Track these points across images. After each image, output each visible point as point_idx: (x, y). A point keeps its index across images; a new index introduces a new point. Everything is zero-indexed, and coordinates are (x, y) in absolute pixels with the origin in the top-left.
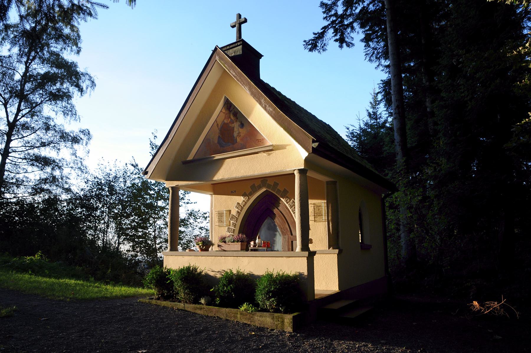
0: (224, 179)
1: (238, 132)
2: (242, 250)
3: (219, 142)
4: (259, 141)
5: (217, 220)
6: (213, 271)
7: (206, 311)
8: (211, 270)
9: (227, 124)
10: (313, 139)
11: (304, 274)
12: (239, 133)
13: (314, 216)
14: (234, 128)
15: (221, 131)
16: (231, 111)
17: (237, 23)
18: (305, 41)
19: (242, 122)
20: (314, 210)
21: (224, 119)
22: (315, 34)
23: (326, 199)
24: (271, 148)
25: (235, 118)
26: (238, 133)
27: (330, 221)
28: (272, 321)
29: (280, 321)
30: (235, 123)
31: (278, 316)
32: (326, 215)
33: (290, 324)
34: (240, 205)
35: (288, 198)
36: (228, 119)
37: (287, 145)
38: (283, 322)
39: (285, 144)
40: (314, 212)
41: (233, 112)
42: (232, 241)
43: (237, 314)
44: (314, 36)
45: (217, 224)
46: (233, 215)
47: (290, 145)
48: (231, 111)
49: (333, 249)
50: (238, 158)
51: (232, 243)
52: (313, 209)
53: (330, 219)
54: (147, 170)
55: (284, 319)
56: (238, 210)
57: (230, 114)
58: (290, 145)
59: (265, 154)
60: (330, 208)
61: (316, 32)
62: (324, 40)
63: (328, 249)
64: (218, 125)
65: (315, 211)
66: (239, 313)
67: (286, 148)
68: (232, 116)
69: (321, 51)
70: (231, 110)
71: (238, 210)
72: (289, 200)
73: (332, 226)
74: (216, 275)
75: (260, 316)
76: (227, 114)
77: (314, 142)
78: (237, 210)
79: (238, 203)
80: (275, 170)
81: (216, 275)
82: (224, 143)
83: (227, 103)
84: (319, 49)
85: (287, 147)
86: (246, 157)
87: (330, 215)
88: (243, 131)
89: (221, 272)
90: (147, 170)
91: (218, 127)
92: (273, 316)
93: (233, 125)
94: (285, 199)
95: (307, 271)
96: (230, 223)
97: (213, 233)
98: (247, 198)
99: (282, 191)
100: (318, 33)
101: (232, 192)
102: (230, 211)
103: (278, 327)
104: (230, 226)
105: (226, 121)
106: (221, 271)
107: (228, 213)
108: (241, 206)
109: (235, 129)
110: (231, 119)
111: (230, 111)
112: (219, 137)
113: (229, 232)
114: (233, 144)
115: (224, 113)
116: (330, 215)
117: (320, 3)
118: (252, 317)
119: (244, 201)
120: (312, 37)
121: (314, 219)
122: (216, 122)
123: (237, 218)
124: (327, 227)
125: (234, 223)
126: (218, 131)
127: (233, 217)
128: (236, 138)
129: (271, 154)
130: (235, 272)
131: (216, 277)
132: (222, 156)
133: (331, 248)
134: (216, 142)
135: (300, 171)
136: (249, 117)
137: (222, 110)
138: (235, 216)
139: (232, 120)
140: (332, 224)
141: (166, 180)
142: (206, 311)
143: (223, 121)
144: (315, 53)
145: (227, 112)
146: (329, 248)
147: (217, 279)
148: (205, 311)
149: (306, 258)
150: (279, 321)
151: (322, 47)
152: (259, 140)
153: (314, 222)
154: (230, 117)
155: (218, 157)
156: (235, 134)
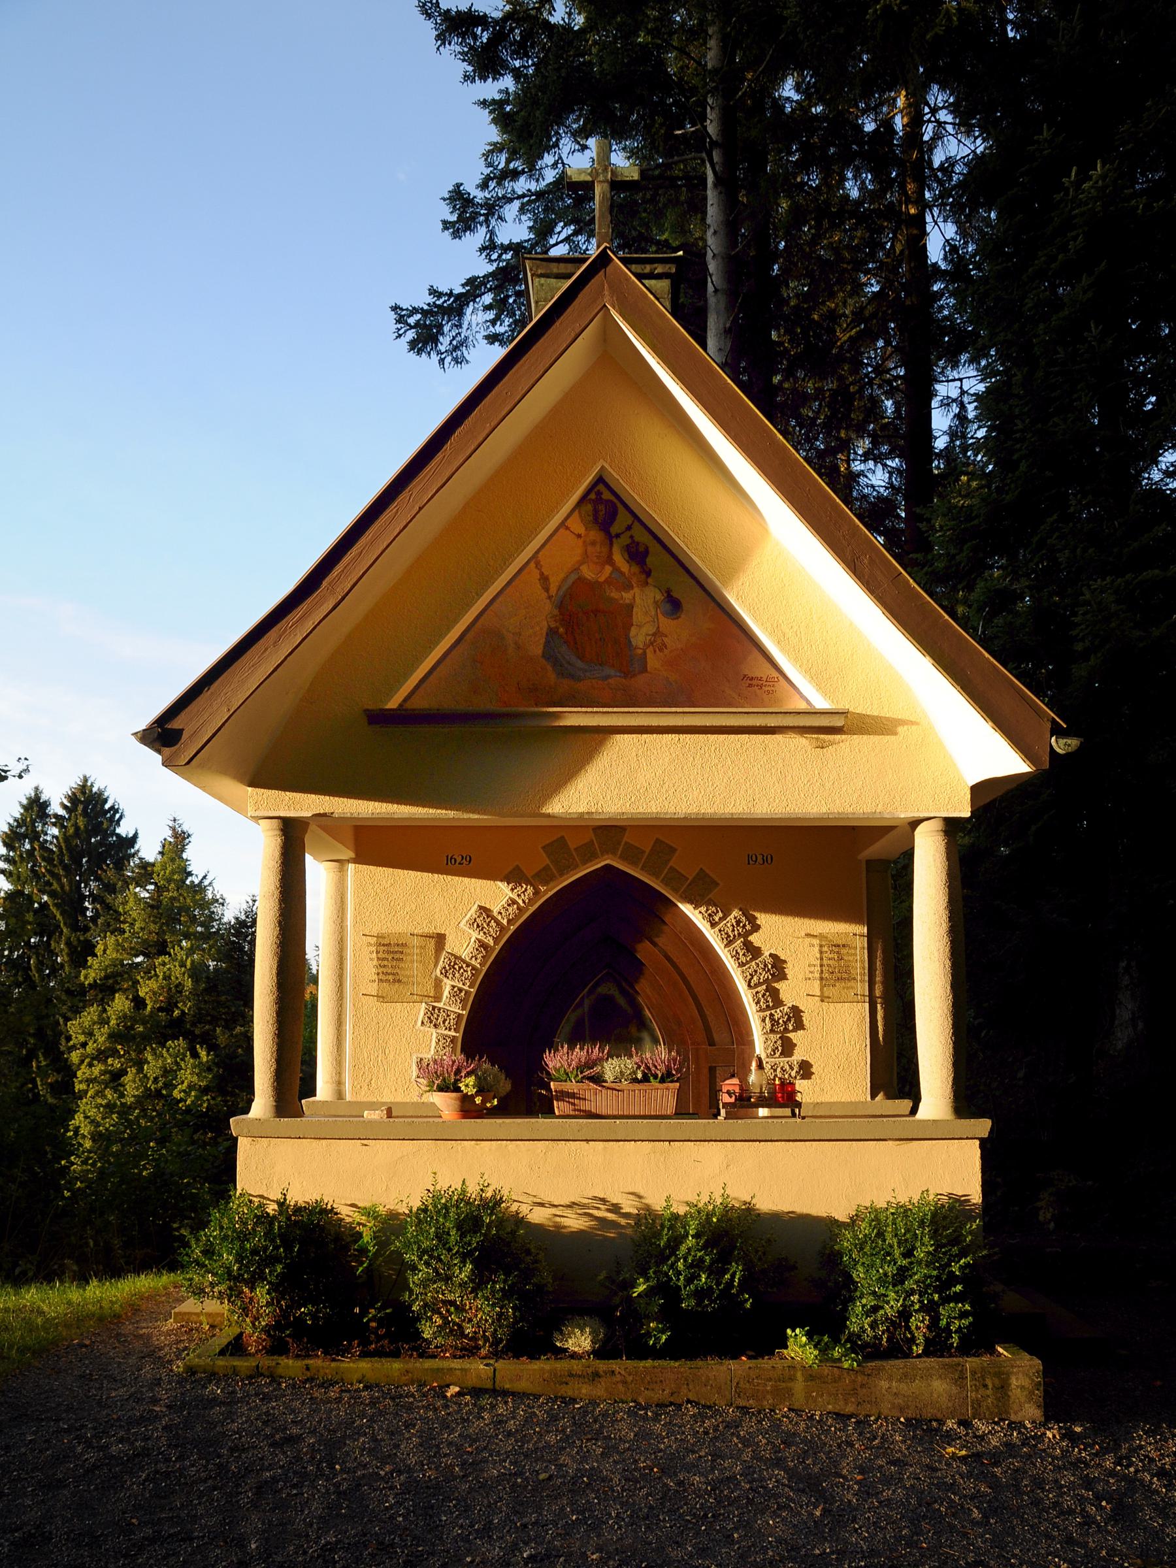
0: (595, 816)
1: (652, 630)
2: (680, 1113)
3: (549, 654)
4: (754, 682)
5: (369, 969)
6: (542, 1205)
7: (624, 1382)
8: (530, 1200)
9: (593, 586)
10: (1053, 721)
11: (968, 1201)
12: (658, 633)
13: (821, 979)
14: (630, 607)
15: (561, 606)
16: (618, 536)
17: (601, 178)
18: (395, 308)
19: (674, 594)
20: (822, 959)
21: (581, 563)
22: (433, 292)
23: (866, 919)
24: (838, 722)
25: (635, 569)
26: (654, 635)
27: (879, 1000)
28: (955, 1390)
29: (990, 1386)
30: (636, 590)
31: (983, 1368)
32: (867, 978)
33: (1031, 1393)
34: (493, 918)
35: (715, 905)
36: (603, 565)
37: (903, 722)
38: (1003, 1388)
39: (886, 713)
40: (821, 966)
41: (625, 540)
42: (640, 1076)
43: (792, 1379)
44: (430, 299)
45: (373, 989)
46: (456, 957)
47: (916, 723)
48: (618, 536)
49: (889, 1096)
50: (675, 737)
51: (637, 1086)
52: (818, 956)
53: (878, 992)
54: (175, 724)
55: (1008, 1378)
56: (481, 936)
57: (611, 544)
58: (912, 723)
59: (801, 742)
60: (879, 953)
61: (444, 289)
62: (465, 326)
63: (869, 1098)
64: (544, 579)
65: (825, 962)
66: (799, 1374)
67: (896, 734)
68: (618, 558)
69: (448, 359)
70: (615, 529)
71: (481, 936)
72: (720, 914)
73: (885, 1018)
74: (558, 1219)
75: (905, 1377)
76: (593, 543)
77: (1056, 731)
78: (475, 935)
79: (481, 907)
80: (850, 810)
81: (558, 1219)
82: (579, 664)
83: (593, 496)
84: (443, 350)
85: (900, 729)
86: (712, 737)
87: (878, 979)
88: (677, 632)
89: (584, 1206)
90: (175, 724)
91: (547, 590)
92: (961, 1371)
93: (627, 596)
94: (703, 909)
95: (979, 1189)
96: (438, 985)
97: (348, 1027)
98: (530, 890)
99: (691, 878)
100: (450, 294)
101: (450, 859)
102: (440, 939)
103: (983, 1409)
104: (438, 998)
105: (588, 572)
106: (586, 1201)
107: (431, 944)
108: (498, 923)
109: (638, 615)
110: (616, 569)
111: (611, 538)
112: (552, 632)
113: (436, 1026)
114: (627, 674)
115: (579, 536)
116: (878, 979)
117: (451, 188)
118: (862, 1386)
119: (514, 902)
120: (423, 300)
121: (822, 990)
122: (538, 565)
123: (474, 968)
124: (868, 1020)
125: (460, 990)
126: (548, 607)
127: (456, 962)
128: (645, 653)
129: (832, 743)
130: (473, 1190)
131: (558, 1226)
132: (596, 716)
133: (880, 1097)
134: (537, 649)
135: (951, 826)
136: (725, 583)
137: (569, 523)
138: (464, 961)
139: (622, 573)
140: (885, 1010)
141: (252, 784)
142: (624, 1382)
143: (576, 569)
144: (429, 362)
145: (595, 535)
146: (873, 1096)
147: (563, 1235)
148: (620, 1387)
149: (977, 1142)
150: (985, 1386)
151: (456, 348)
152: (752, 679)
153: (819, 1003)
154: (609, 560)
155: (575, 717)
156: (639, 637)
